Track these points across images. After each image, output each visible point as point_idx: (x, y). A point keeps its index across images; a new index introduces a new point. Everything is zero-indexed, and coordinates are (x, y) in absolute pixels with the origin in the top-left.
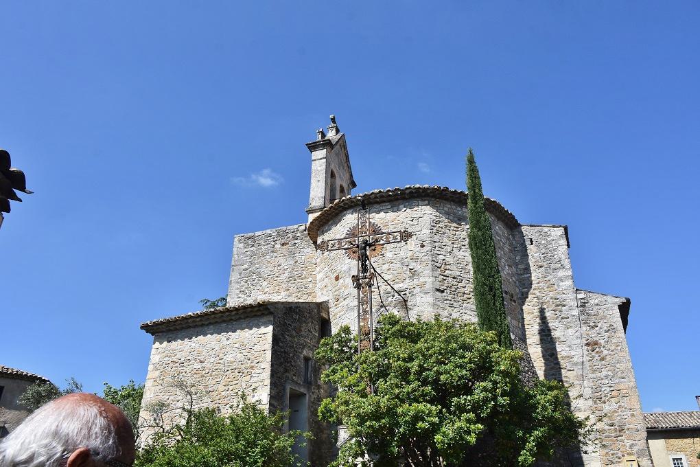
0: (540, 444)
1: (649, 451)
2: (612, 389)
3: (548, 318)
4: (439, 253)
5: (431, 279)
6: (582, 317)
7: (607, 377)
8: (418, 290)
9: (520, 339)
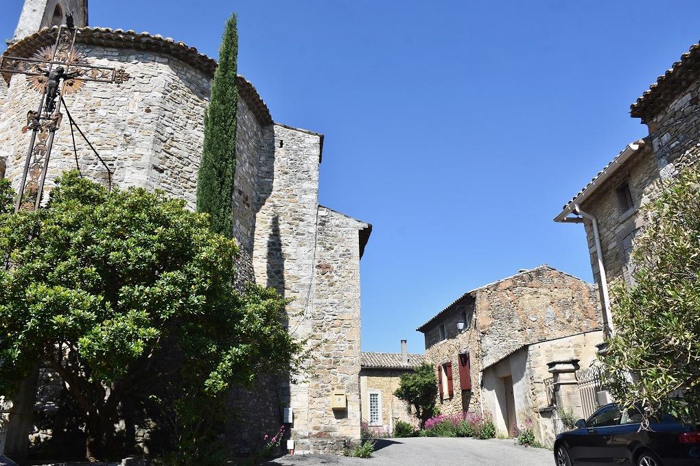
0: (239, 366)
1: (359, 385)
2: (335, 317)
3: (282, 231)
4: (167, 124)
5: (150, 152)
6: (319, 236)
7: (332, 304)
8: (130, 162)
9: (245, 249)
